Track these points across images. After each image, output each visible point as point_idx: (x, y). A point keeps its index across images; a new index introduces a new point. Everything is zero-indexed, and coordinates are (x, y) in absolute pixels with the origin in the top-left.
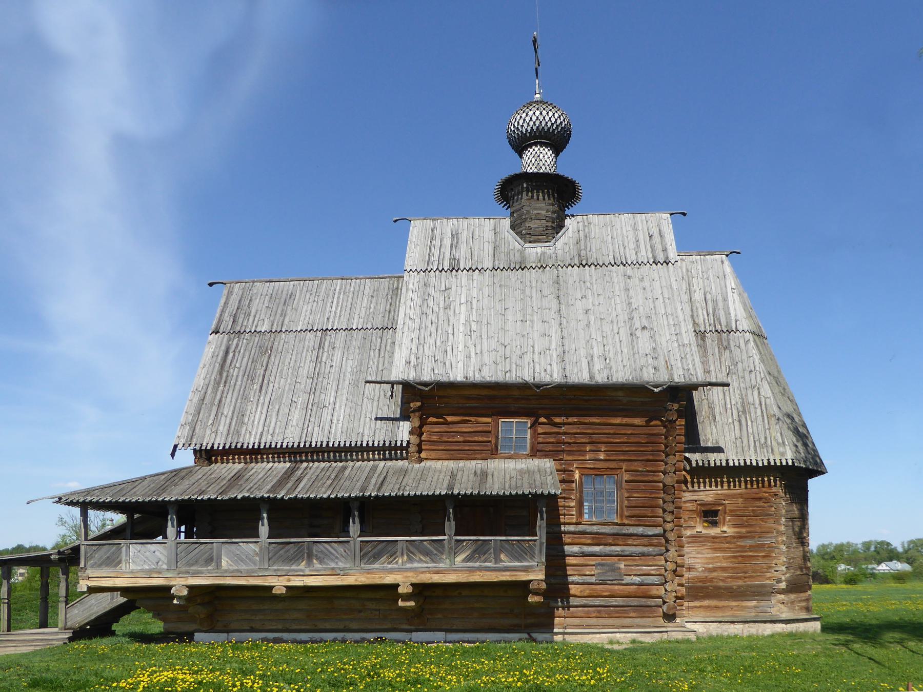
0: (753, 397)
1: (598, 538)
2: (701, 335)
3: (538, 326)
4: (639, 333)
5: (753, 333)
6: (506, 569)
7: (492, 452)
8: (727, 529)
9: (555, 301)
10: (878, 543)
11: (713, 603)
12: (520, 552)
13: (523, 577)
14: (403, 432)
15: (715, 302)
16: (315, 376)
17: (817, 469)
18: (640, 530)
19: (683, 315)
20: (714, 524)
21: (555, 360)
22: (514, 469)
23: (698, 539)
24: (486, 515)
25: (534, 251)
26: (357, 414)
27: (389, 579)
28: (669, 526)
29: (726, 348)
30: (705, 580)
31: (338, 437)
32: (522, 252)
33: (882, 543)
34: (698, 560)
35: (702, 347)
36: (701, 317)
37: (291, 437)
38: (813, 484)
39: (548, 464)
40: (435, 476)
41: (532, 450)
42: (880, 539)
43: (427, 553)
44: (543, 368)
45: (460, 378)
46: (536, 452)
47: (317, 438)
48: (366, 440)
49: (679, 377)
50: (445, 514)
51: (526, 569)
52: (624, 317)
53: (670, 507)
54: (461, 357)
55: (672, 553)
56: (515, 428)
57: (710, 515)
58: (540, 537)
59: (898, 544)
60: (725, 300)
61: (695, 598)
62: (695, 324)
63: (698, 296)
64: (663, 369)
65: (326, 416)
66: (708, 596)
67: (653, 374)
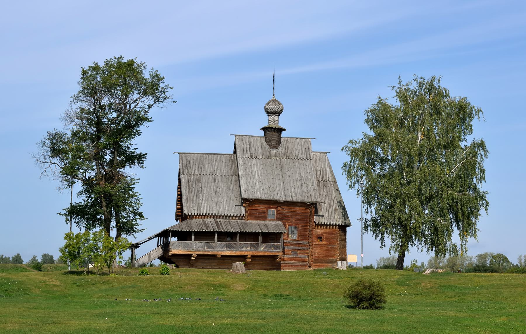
0: (332, 203)
1: (292, 244)
2: (319, 182)
3: (277, 181)
4: (303, 185)
5: (333, 182)
6: (273, 252)
7: (265, 218)
8: (324, 243)
9: (281, 172)
10: (494, 257)
11: (321, 264)
12: (276, 247)
13: (277, 254)
14: (243, 211)
15: (323, 170)
16: (216, 192)
17: (349, 225)
18: (302, 242)
19: (314, 176)
20: (321, 240)
21: (283, 193)
22: (272, 225)
23: (316, 245)
24: (271, 237)
25: (273, 152)
26: (229, 206)
27: (246, 254)
28: (310, 241)
29: (326, 187)
30: (318, 257)
31: (227, 213)
32: (270, 152)
33: (499, 256)
34: (317, 251)
35: (319, 186)
36: (319, 176)
37: (215, 212)
38: (348, 229)
39: (280, 223)
40: (255, 226)
41: (276, 218)
42: (495, 253)
43: (255, 247)
44: (280, 196)
45: (259, 198)
46: (277, 219)
47: (222, 213)
48: (234, 214)
49: (314, 200)
50: (259, 235)
51: (278, 252)
52: (299, 179)
53: (310, 236)
54: (258, 190)
55: (311, 249)
56: (272, 212)
57: (320, 238)
58: (281, 243)
59: (514, 260)
60: (326, 170)
61: (315, 263)
62: (317, 178)
63: (318, 168)
64: (309, 197)
65: (222, 206)
66: (319, 262)
67: (307, 199)
